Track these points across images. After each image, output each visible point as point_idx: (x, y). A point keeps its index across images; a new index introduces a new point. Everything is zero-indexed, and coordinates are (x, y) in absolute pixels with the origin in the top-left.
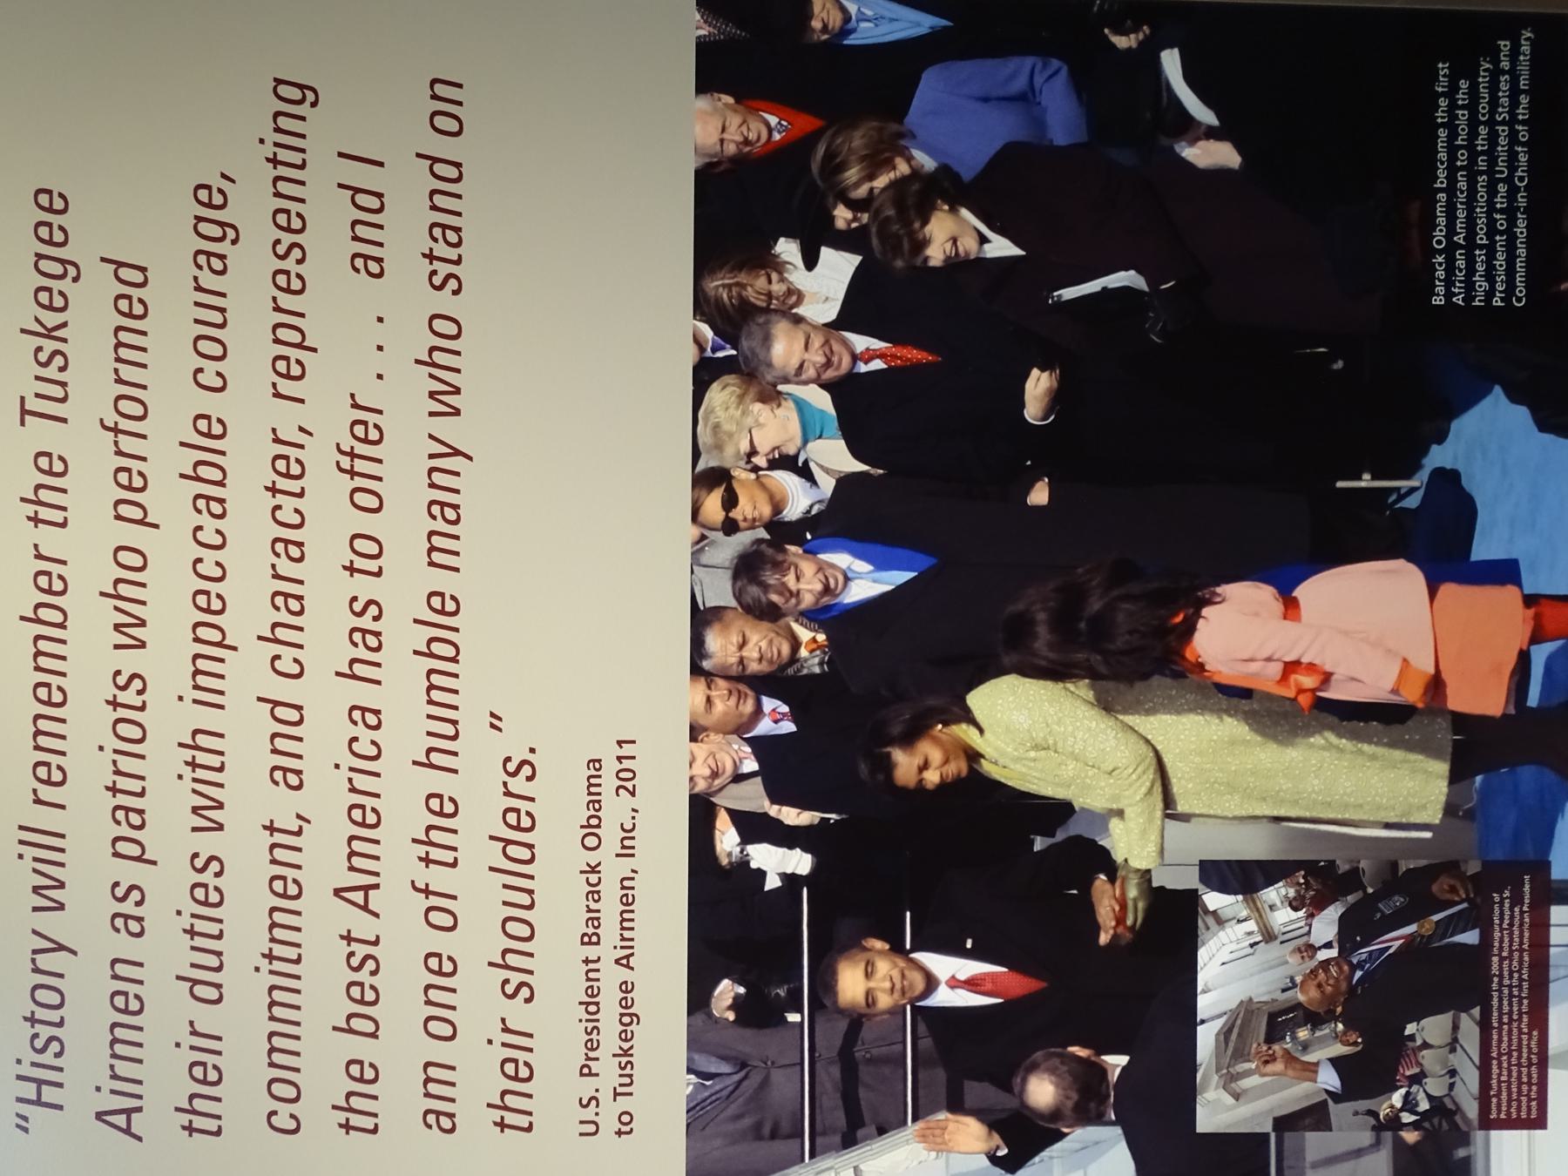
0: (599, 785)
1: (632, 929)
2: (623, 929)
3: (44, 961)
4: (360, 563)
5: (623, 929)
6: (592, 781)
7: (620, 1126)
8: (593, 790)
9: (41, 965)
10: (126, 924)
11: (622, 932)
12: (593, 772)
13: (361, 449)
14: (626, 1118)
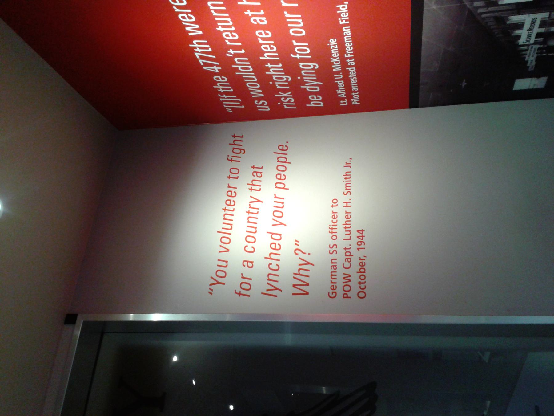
0: (336, 275)
1: (336, 279)
2: (332, 278)
3: (253, 205)
4: (232, 175)
5: (332, 278)
6: (333, 274)
7: (333, 204)
8: (348, 188)
9: (252, 206)
10: (275, 247)
11: (331, 280)
12: (333, 270)
13: (228, 208)
14: (335, 201)
